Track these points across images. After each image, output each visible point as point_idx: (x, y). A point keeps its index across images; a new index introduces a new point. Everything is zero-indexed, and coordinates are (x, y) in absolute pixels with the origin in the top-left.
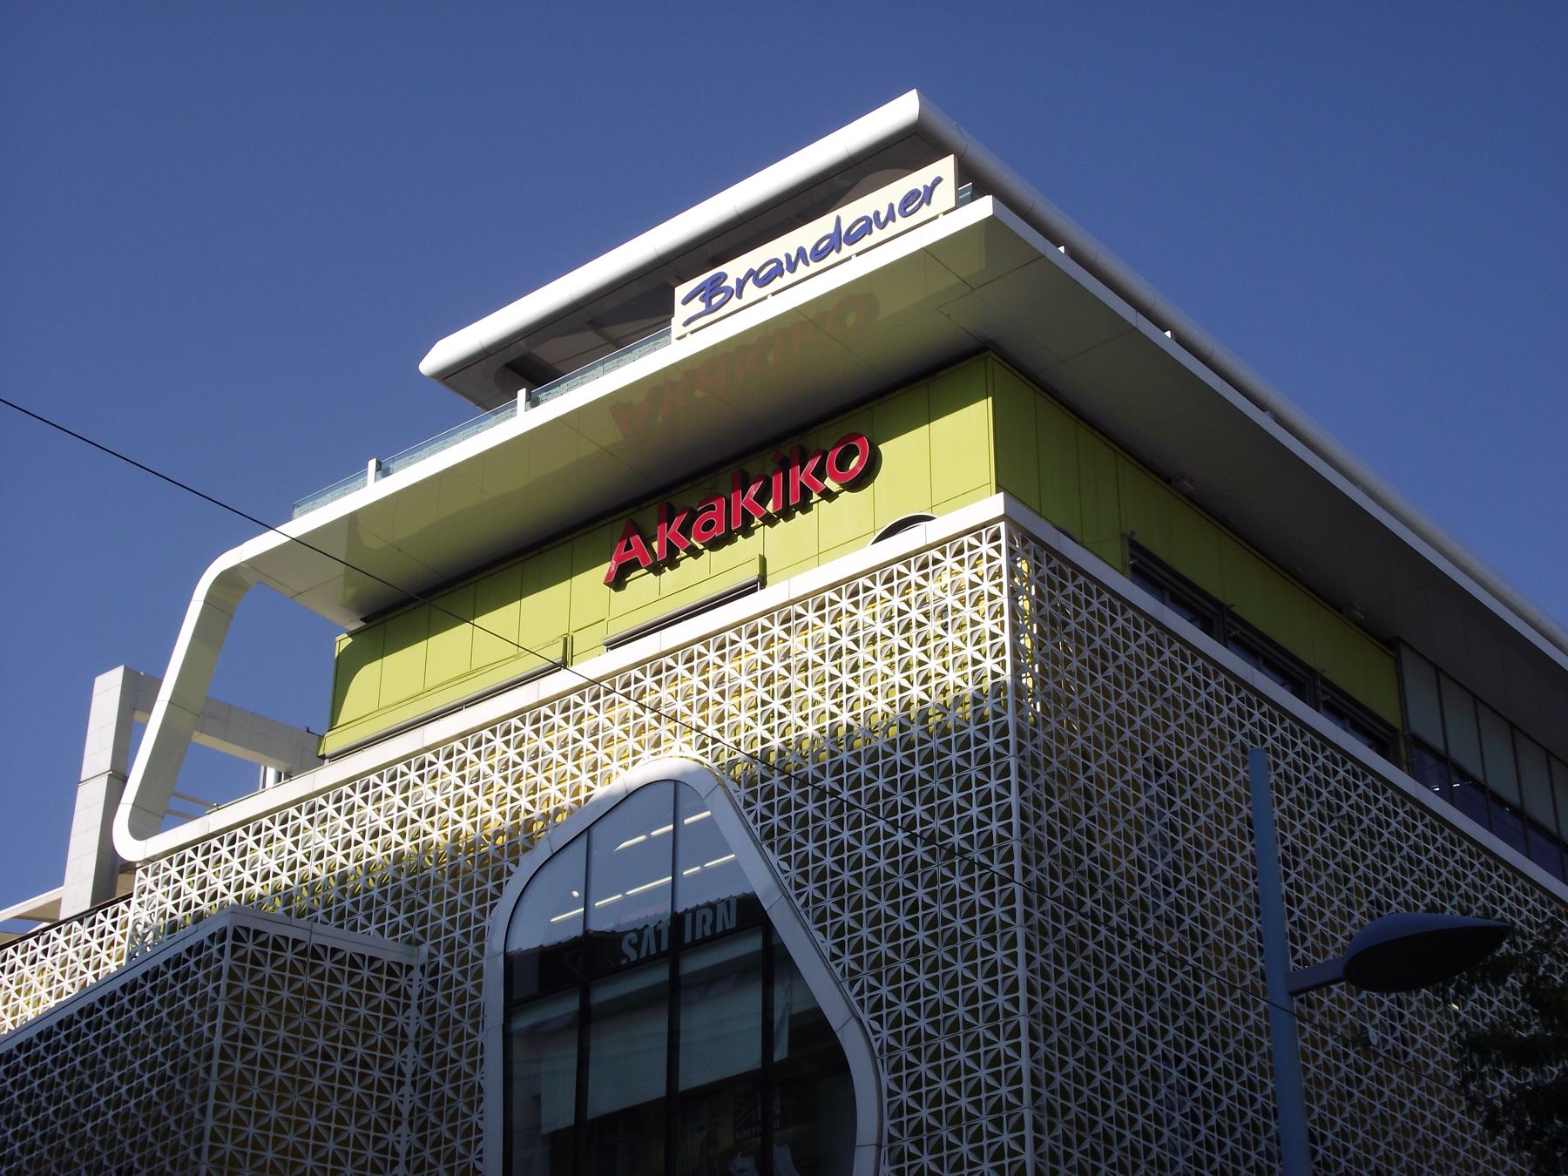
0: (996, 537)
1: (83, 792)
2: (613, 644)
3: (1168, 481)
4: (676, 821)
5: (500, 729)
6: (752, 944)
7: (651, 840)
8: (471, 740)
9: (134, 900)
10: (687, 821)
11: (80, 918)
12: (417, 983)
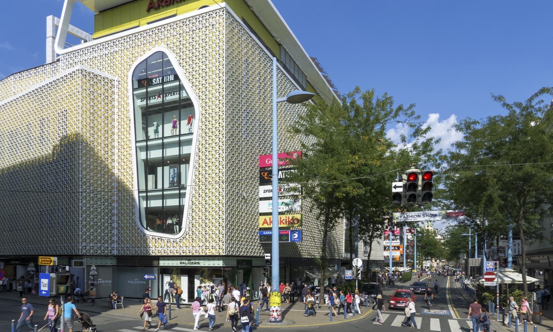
0: (223, 11)
1: (47, 40)
2: (148, 23)
3: (249, 7)
4: (163, 59)
5: (72, 53)
6: (177, 83)
7: (157, 62)
8: (175, 24)
9: (60, 62)
10: (129, 282)
11: (50, 64)
12: (116, 83)
